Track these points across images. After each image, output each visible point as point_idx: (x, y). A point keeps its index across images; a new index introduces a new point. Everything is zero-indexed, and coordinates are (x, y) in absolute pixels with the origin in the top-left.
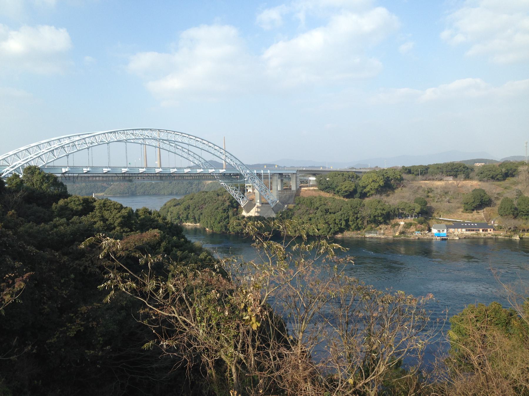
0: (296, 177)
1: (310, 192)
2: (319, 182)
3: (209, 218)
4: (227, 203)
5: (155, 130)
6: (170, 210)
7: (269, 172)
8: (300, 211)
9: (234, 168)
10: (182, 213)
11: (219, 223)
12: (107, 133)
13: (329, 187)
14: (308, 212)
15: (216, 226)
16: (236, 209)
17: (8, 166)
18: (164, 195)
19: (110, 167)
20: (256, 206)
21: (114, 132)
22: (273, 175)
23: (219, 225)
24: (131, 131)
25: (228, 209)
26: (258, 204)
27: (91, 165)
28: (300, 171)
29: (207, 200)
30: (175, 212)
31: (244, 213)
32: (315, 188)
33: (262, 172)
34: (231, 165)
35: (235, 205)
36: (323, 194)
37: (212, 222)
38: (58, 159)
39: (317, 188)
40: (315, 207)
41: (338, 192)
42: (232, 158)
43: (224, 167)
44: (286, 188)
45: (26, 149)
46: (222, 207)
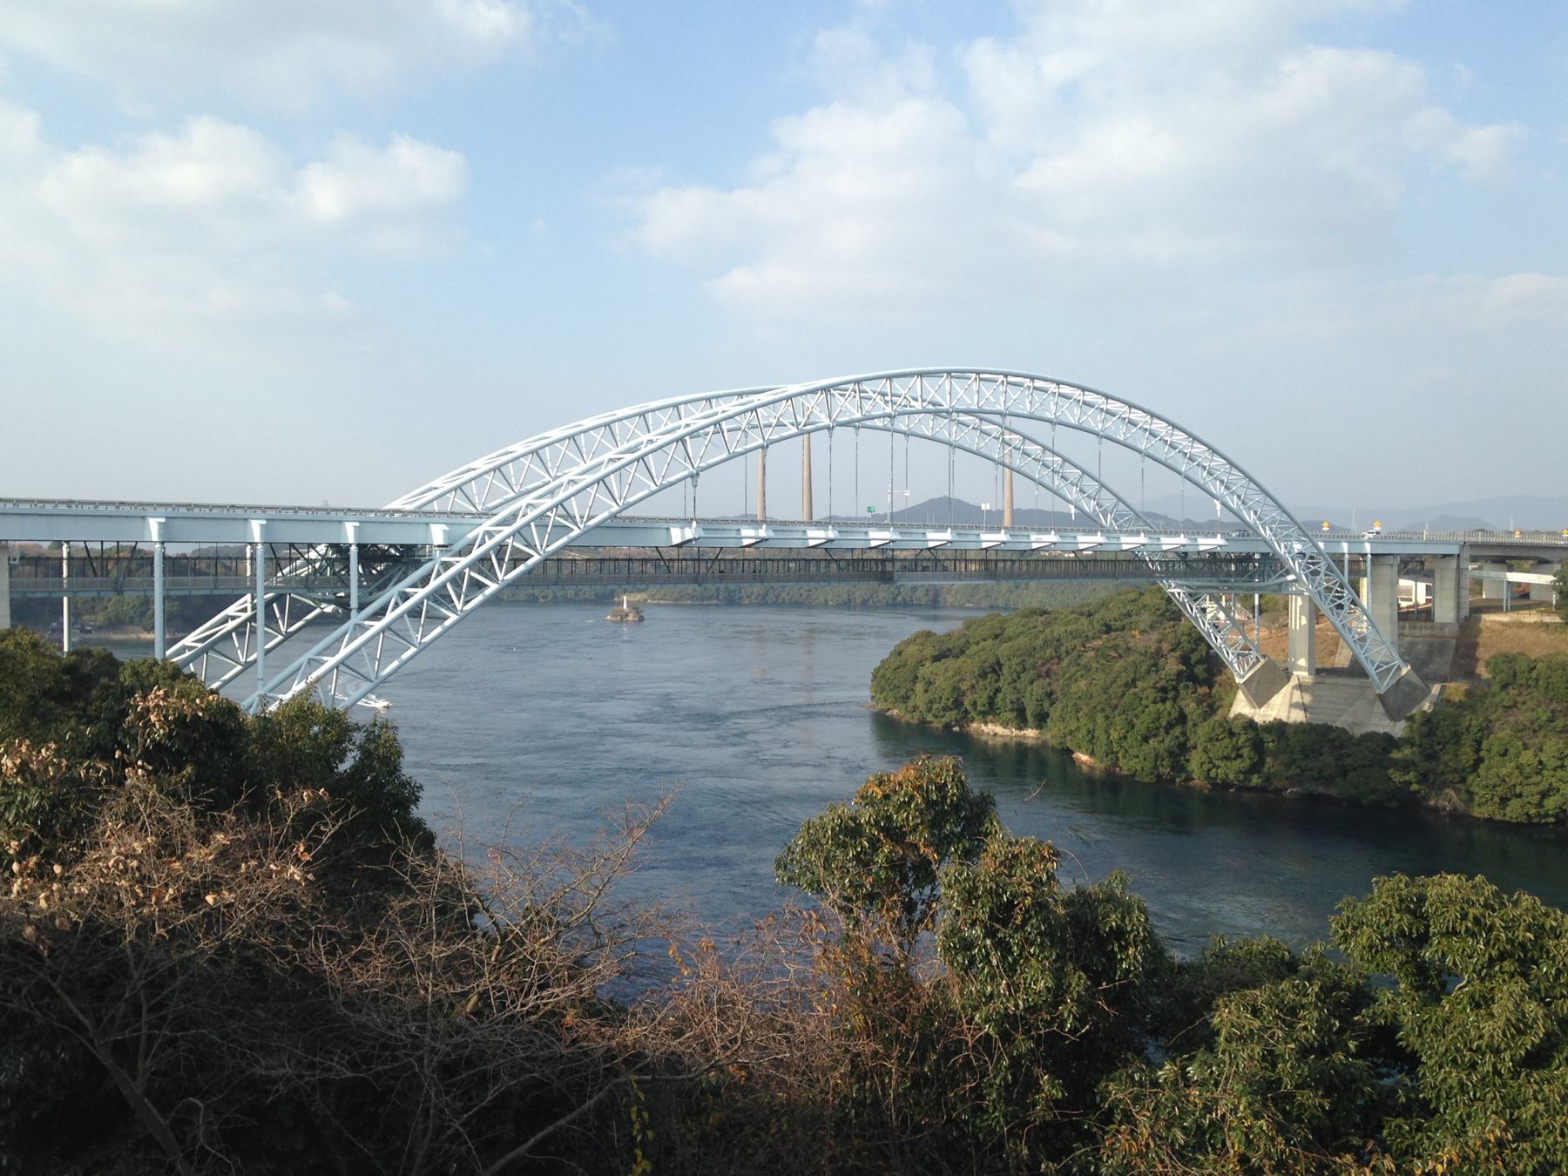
0: (1459, 571)
1: (1522, 632)
3: (1100, 719)
4: (1172, 666)
5: (961, 374)
6: (922, 672)
11: (1146, 740)
12: (685, 403)
18: (826, 605)
19: (770, 523)
20: (1294, 682)
25: (1175, 688)
26: (1302, 674)
28: (1474, 546)
29: (1067, 645)
30: (943, 684)
31: (1241, 706)
32: (1547, 619)
33: (1345, 547)
37: (1114, 735)
38: (662, 488)
39: (1557, 619)
43: (1007, 522)
45: (535, 452)
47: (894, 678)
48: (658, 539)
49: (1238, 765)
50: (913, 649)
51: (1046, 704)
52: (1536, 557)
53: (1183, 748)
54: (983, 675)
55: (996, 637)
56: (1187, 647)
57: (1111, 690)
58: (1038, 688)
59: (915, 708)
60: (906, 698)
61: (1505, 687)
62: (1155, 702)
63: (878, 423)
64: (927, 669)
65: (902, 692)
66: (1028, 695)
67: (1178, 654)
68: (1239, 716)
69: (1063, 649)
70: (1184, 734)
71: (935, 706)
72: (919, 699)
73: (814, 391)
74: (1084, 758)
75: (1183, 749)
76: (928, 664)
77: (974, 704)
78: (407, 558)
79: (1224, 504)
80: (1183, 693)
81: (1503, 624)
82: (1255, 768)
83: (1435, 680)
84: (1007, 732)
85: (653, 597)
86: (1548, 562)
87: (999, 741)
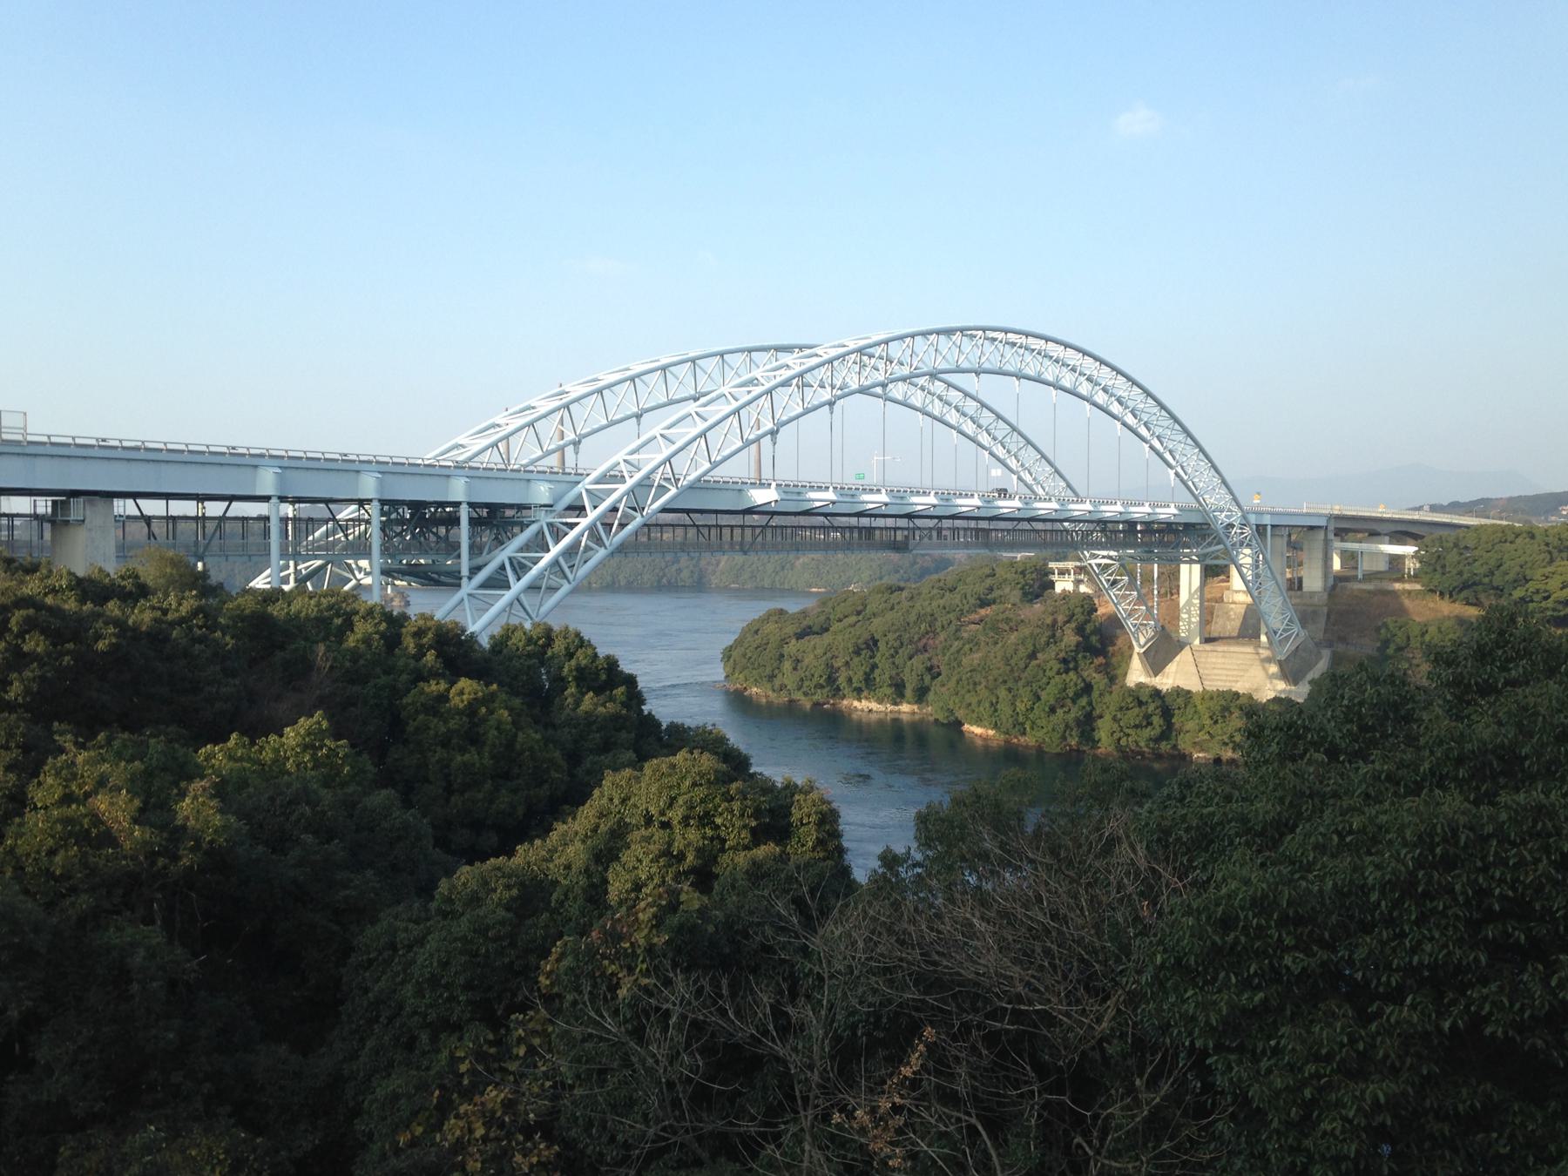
3: (1002, 693)
4: (1070, 638)
6: (786, 650)
11: (1053, 710)
25: (1075, 659)
27: (837, 479)
31: (1137, 675)
37: (1021, 707)
39: (1418, 587)
49: (1147, 733)
50: (770, 627)
51: (927, 678)
52: (1402, 531)
54: (857, 653)
55: (859, 613)
56: (1081, 618)
57: (1013, 662)
58: (918, 663)
59: (783, 687)
60: (771, 677)
62: (1058, 673)
64: (793, 647)
65: (768, 671)
66: (907, 670)
67: (1073, 625)
68: (1140, 686)
69: (938, 624)
70: (1090, 703)
71: (806, 683)
72: (788, 677)
74: (978, 730)
75: (1087, 724)
76: (794, 641)
77: (850, 680)
79: (1020, 478)
80: (1081, 663)
81: (1369, 592)
82: (1165, 735)
84: (881, 708)
86: (1378, 534)
87: (874, 717)
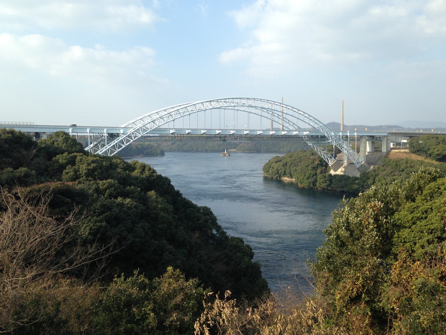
0: (387, 139)
2: (411, 145)
4: (317, 162)
5: (244, 99)
7: (356, 134)
8: (385, 172)
9: (318, 131)
10: (281, 169)
11: (308, 179)
13: (421, 150)
14: (393, 174)
15: (305, 182)
16: (324, 168)
17: (132, 128)
21: (210, 101)
22: (360, 138)
23: (308, 181)
24: (224, 100)
25: (317, 168)
28: (392, 134)
29: (303, 158)
30: (275, 168)
31: (332, 172)
34: (315, 128)
35: (324, 165)
36: (414, 157)
37: (301, 178)
40: (401, 169)
41: (430, 155)
42: (316, 121)
44: (376, 149)
46: (311, 166)
47: (267, 168)
48: (168, 132)
49: (325, 184)
53: (316, 181)
60: (268, 172)
61: (383, 166)
63: (230, 108)
70: (316, 177)
73: (207, 102)
78: (118, 135)
82: (329, 185)
83: (372, 165)
85: (237, 150)
87: (287, 181)
